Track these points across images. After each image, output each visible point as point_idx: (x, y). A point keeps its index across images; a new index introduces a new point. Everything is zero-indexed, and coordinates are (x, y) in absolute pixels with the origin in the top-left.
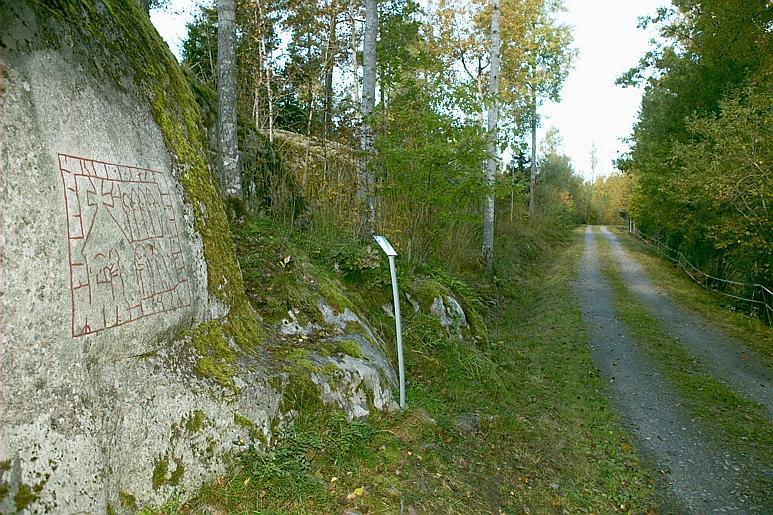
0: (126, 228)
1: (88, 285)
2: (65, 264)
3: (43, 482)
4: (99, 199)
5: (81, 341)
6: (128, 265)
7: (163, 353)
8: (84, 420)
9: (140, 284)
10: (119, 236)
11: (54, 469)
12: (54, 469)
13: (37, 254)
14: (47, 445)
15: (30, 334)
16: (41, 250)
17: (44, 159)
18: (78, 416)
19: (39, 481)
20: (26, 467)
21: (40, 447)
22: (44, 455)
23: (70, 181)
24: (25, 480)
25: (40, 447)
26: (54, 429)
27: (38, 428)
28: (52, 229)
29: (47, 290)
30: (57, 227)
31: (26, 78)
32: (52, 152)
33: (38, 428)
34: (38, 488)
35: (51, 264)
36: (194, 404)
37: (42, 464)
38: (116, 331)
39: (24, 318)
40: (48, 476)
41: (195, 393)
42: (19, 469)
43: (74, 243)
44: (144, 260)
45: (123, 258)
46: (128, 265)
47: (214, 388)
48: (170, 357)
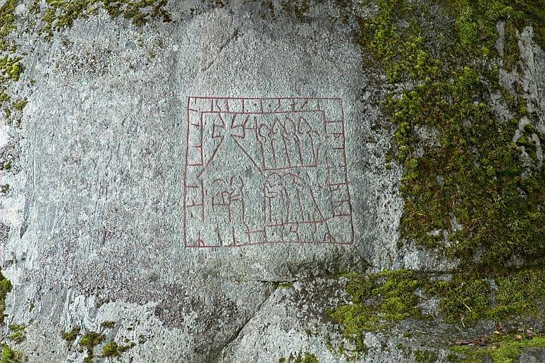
0: (257, 157)
1: (203, 205)
2: (179, 186)
3: (128, 348)
4: (226, 132)
5: (195, 252)
7: (297, 286)
8: (188, 320)
9: (267, 211)
10: (245, 163)
11: (141, 342)
12: (141, 342)
13: (155, 177)
14: (145, 324)
15: (147, 236)
16: (158, 173)
17: (175, 102)
18: (183, 314)
19: (126, 345)
20: (122, 332)
21: (139, 323)
22: (140, 330)
23: (195, 118)
24: (116, 340)
25: (139, 323)
26: (156, 315)
27: (143, 311)
28: (171, 158)
29: (162, 205)
30: (175, 156)
31: (178, 41)
32: (182, 97)
33: (143, 311)
34: (124, 349)
35: (167, 185)
36: (307, 344)
37: (133, 336)
38: (235, 251)
39: (141, 223)
40: (133, 345)
41: (309, 333)
42: (116, 332)
43: (191, 169)
44: (277, 189)
45: (248, 185)
47: (333, 336)
48: (304, 291)
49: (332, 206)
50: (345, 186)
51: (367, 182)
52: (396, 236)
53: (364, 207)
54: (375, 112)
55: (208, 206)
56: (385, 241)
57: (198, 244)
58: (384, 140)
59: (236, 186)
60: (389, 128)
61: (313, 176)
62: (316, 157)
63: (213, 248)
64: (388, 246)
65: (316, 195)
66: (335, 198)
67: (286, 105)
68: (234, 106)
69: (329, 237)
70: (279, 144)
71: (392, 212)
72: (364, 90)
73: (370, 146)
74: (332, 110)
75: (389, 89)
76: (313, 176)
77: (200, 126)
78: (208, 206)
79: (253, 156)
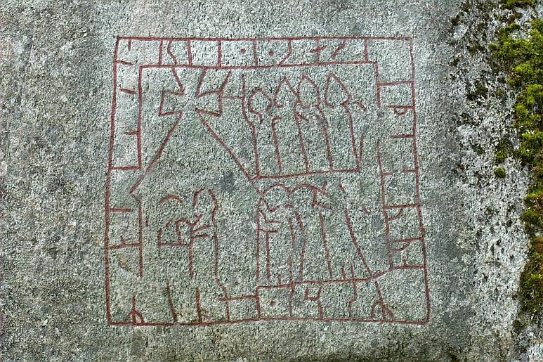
6: (235, 223)
10: (219, 164)
16: (58, 184)
23: (127, 78)
38: (201, 333)
43: (118, 176)
46: (235, 223)
49: (389, 248)
50: (414, 210)
51: (457, 199)
52: (512, 309)
53: (452, 251)
54: (477, 65)
55: (150, 248)
56: (490, 318)
57: (133, 318)
58: (493, 119)
59: (204, 209)
60: (502, 96)
61: (351, 189)
62: (358, 153)
63: (162, 326)
64: (496, 327)
65: (357, 226)
66: (394, 233)
67: (303, 50)
68: (204, 53)
69: (383, 310)
70: (287, 128)
71: (507, 257)
72: (455, 22)
73: (465, 132)
74: (394, 60)
75: (503, 19)
76: (351, 189)
77: (138, 92)
79: (237, 150)
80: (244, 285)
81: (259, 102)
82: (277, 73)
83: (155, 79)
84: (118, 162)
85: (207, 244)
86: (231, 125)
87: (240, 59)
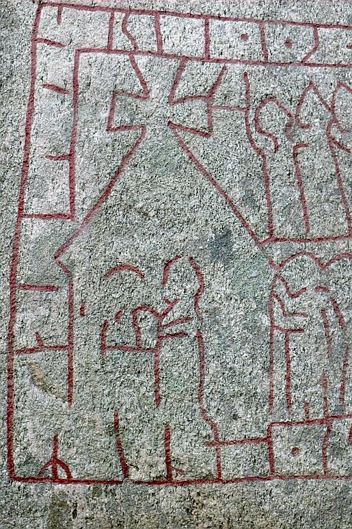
6: (233, 314)
10: (209, 215)
23: (55, 66)
43: (35, 229)
46: (233, 314)
55: (87, 353)
63: (100, 484)
77: (72, 91)
78: (87, 353)
79: (237, 194)
80: (248, 421)
81: (272, 118)
82: (302, 74)
83: (101, 72)
84: (34, 206)
85: (183, 345)
86: (227, 150)
87: (240, 49)
